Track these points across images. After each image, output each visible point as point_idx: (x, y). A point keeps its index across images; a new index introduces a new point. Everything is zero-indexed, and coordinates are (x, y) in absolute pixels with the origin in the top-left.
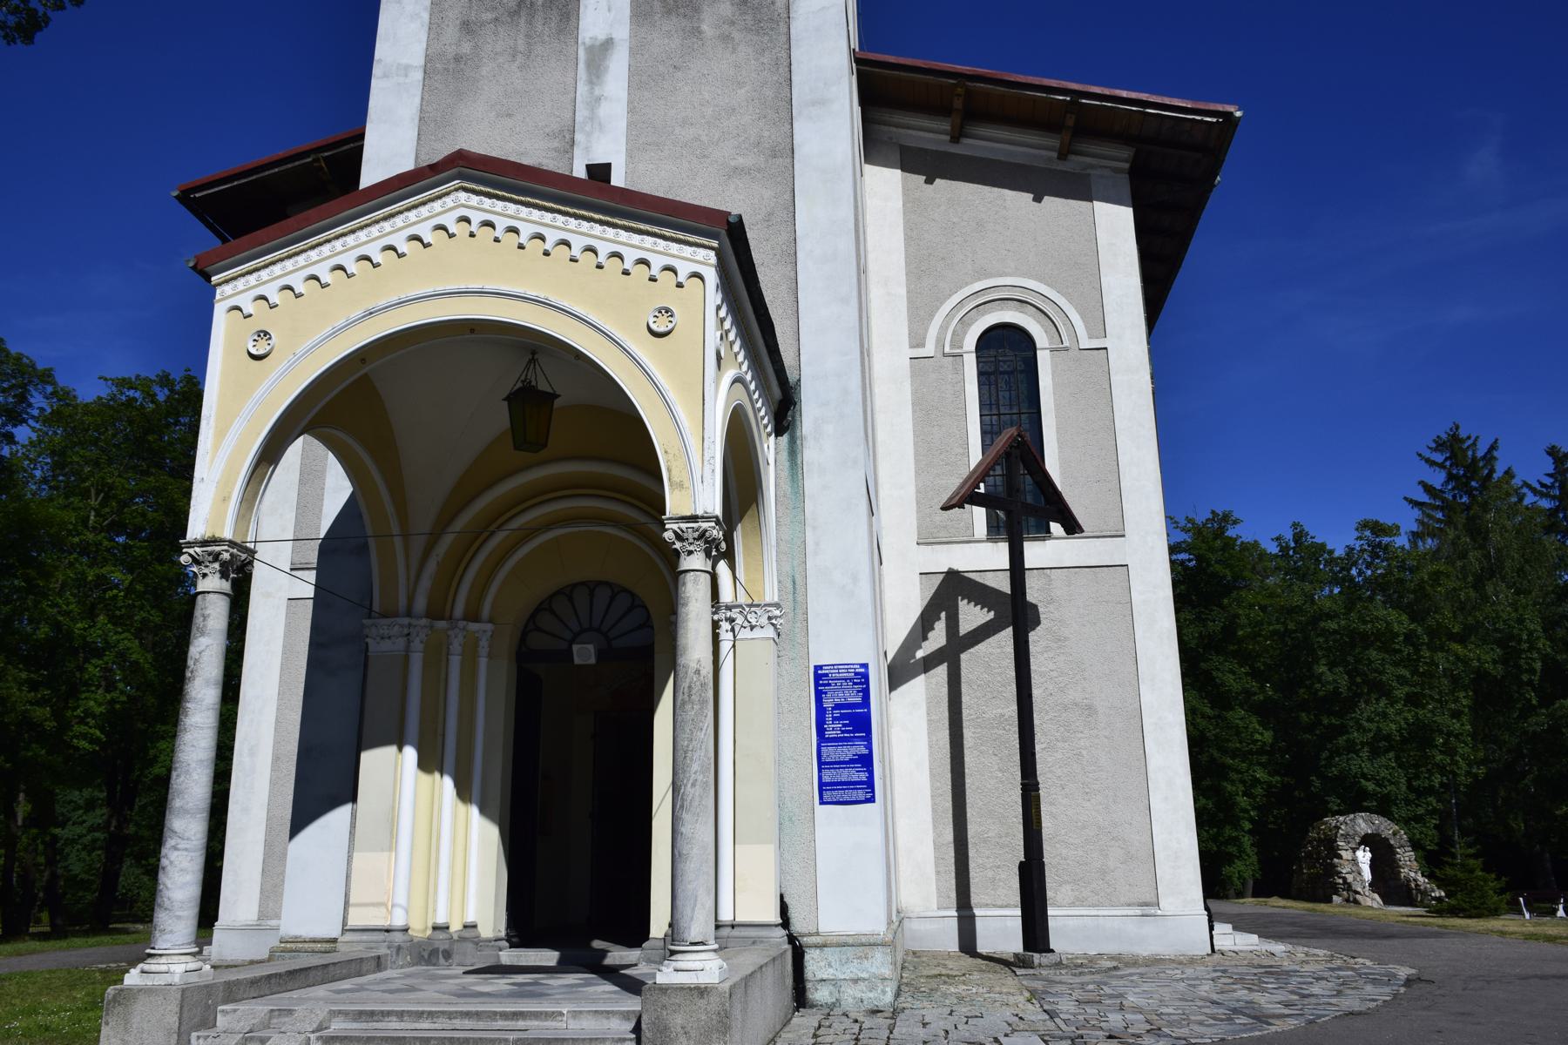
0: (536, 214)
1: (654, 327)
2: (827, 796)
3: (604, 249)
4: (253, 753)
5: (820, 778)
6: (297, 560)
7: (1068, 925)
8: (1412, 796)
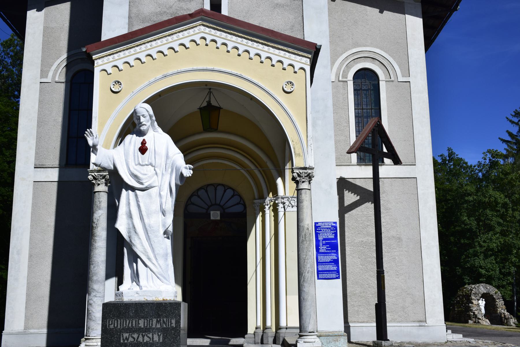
0: (234, 38)
1: (285, 89)
2: (320, 276)
3: (242, 48)
4: (19, 253)
5: (317, 268)
6: (37, 163)
7: (394, 330)
8: (501, 276)
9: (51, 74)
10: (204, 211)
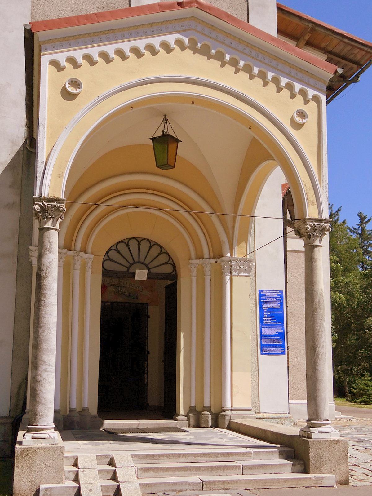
5: (261, 342)
10: (125, 269)
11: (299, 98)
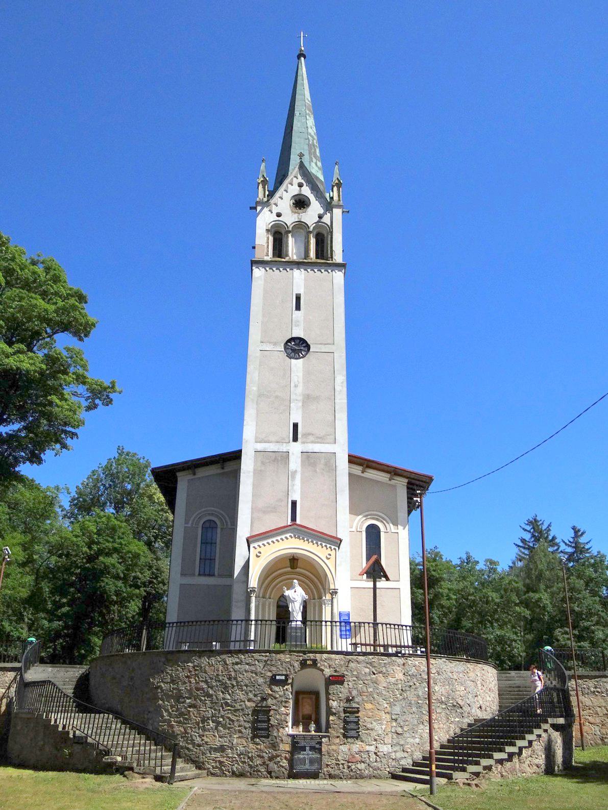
9: (190, 522)
11: (329, 549)
